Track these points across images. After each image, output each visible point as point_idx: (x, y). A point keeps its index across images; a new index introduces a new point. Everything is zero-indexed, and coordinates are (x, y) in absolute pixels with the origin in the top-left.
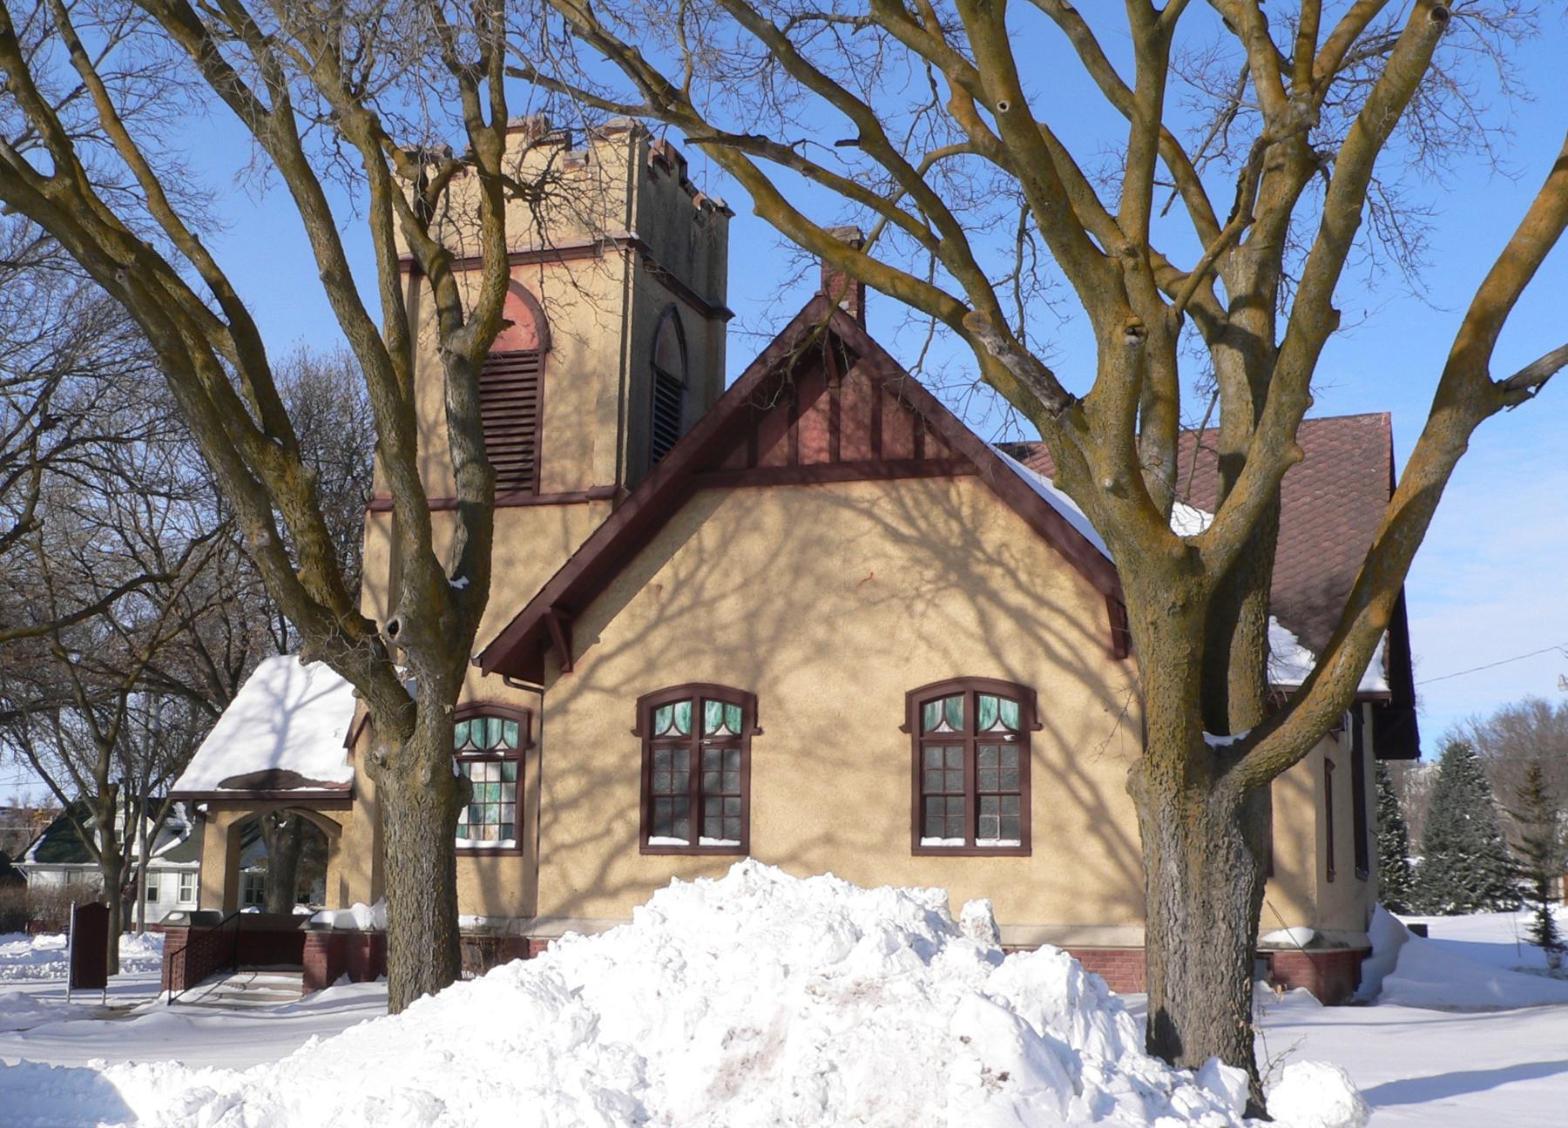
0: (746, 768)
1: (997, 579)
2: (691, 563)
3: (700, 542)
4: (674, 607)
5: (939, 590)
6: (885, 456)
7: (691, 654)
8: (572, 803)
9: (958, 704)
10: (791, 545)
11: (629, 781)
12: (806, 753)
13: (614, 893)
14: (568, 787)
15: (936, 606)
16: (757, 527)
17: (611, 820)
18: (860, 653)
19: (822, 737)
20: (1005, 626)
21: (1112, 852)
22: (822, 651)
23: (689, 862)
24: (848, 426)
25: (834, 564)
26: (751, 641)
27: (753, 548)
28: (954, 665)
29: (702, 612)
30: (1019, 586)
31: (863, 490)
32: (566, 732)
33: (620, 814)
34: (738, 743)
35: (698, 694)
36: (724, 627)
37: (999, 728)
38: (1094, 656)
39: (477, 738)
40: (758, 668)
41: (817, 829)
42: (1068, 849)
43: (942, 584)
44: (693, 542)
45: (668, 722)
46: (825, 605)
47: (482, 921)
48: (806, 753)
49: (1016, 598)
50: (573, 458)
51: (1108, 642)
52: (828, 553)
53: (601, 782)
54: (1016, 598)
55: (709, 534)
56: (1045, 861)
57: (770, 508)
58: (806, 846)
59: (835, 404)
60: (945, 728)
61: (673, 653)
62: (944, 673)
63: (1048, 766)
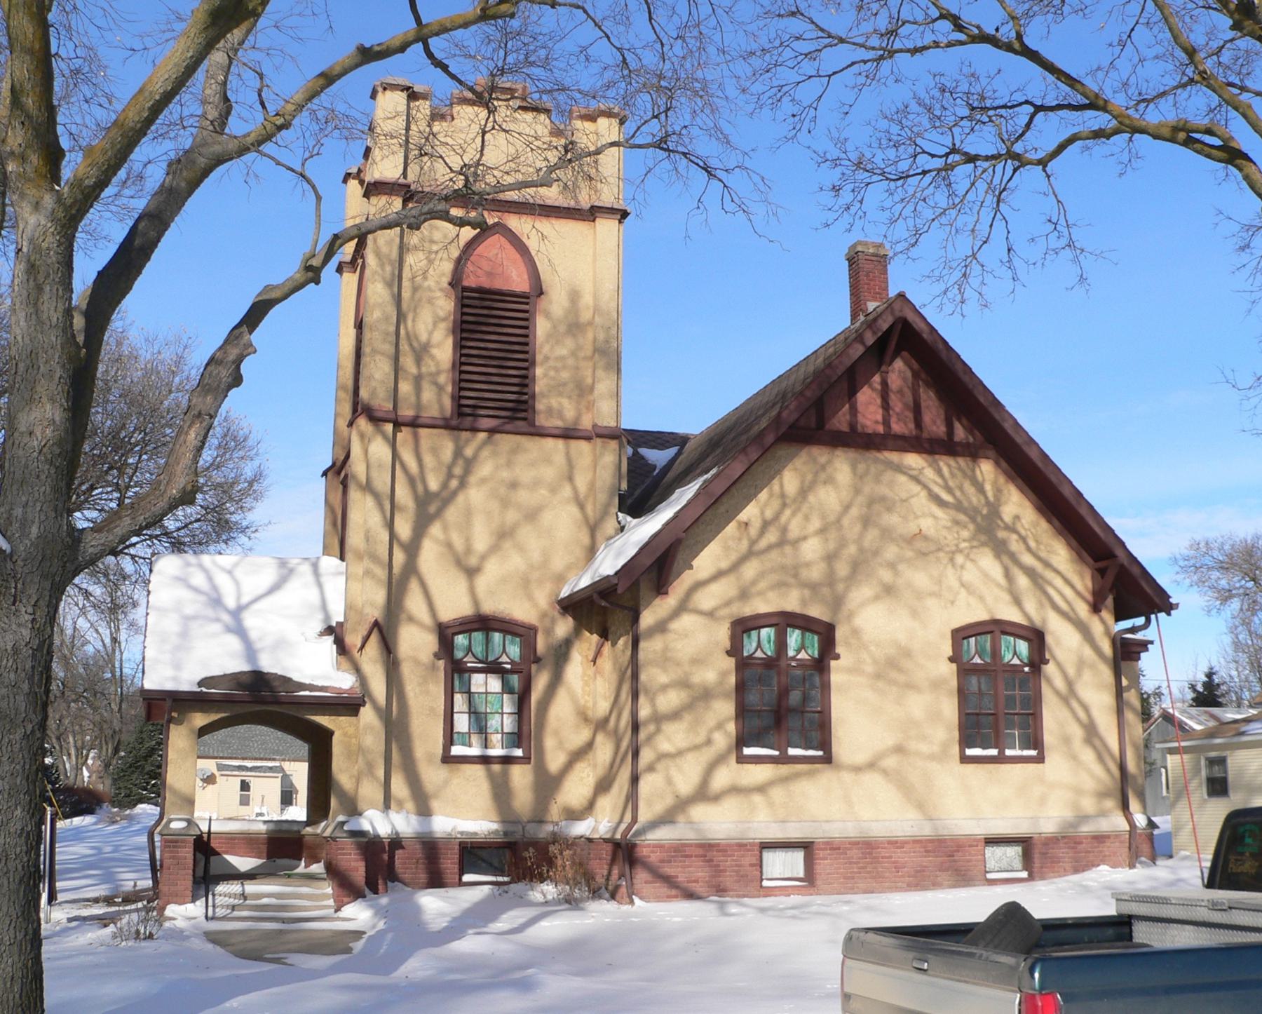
0: (826, 687)
1: (1015, 545)
2: (776, 504)
3: (782, 486)
4: (763, 543)
5: (972, 547)
6: (925, 435)
7: (781, 585)
8: (675, 715)
9: (986, 641)
10: (861, 499)
11: (726, 696)
12: (878, 676)
13: (716, 798)
14: (670, 700)
15: (972, 560)
16: (830, 481)
17: (711, 731)
18: (919, 595)
19: (892, 663)
20: (1023, 581)
21: (1100, 759)
22: (888, 590)
23: (784, 769)
24: (897, 404)
25: (892, 519)
26: (831, 580)
27: (828, 498)
28: (989, 611)
29: (788, 549)
30: (1029, 549)
31: (913, 460)
32: (666, 649)
33: (720, 726)
34: (821, 665)
35: (785, 621)
36: (808, 565)
37: (1016, 661)
38: (1083, 610)
39: (478, 649)
40: (837, 603)
41: (890, 741)
42: (1074, 758)
43: (975, 543)
44: (775, 484)
45: (754, 645)
46: (891, 552)
47: (494, 826)
48: (878, 676)
49: (1028, 559)
50: (570, 397)
51: (1089, 597)
52: (889, 510)
53: (705, 695)
54: (1028, 559)
55: (789, 480)
56: (1056, 765)
57: (842, 466)
58: (881, 756)
59: (884, 384)
60: (977, 660)
61: (762, 585)
62: (981, 615)
63: (1057, 692)
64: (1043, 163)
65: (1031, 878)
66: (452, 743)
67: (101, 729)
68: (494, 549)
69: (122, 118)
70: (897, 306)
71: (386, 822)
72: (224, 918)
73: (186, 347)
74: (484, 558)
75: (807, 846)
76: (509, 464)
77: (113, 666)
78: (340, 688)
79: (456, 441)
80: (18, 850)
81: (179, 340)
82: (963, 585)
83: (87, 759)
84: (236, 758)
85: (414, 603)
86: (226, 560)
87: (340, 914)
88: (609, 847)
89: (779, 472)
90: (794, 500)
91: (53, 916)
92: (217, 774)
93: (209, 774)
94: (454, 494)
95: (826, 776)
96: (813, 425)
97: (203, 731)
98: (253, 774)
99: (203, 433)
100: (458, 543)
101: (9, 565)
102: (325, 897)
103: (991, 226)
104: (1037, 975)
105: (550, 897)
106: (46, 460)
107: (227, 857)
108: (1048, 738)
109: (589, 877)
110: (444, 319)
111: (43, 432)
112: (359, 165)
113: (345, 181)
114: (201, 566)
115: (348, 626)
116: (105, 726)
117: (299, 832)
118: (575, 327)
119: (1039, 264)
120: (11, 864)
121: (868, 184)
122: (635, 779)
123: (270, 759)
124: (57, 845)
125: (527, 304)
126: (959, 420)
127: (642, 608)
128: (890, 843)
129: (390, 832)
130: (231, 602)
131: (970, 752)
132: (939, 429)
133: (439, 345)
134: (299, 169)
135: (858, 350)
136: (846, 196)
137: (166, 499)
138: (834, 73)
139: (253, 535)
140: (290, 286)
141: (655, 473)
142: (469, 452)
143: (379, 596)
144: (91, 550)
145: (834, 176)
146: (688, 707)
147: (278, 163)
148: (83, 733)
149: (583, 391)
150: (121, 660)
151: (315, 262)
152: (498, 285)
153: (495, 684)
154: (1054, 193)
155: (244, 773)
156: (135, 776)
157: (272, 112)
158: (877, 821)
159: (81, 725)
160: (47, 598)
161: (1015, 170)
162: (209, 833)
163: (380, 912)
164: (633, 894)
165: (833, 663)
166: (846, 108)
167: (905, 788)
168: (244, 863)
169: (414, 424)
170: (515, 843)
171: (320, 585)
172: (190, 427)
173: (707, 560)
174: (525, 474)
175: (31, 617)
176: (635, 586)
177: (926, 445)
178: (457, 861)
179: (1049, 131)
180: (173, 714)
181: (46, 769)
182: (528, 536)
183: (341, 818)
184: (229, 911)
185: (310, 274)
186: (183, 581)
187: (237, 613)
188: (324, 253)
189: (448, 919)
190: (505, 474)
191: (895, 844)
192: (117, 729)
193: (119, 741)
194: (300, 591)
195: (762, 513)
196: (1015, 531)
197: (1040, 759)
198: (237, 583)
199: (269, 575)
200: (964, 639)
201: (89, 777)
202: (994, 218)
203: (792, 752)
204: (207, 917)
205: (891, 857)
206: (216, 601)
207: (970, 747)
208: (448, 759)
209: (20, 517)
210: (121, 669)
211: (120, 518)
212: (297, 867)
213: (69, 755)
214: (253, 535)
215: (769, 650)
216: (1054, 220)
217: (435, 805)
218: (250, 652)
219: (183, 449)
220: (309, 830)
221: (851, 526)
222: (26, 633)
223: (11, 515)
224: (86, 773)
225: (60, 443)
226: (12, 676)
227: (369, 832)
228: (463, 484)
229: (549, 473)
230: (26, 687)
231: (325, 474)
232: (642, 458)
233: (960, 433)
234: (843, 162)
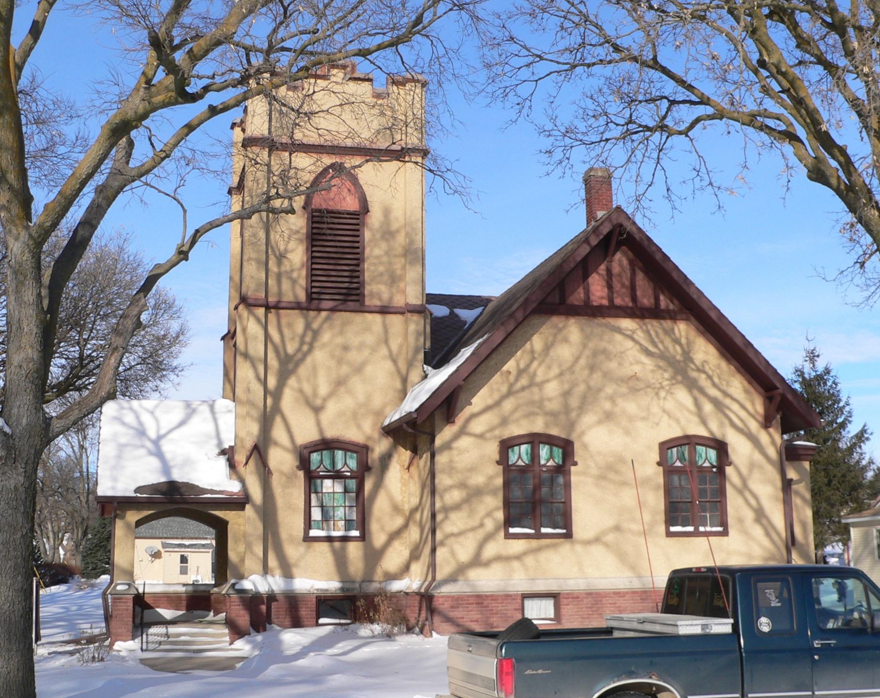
0: (568, 486)
1: (703, 380)
4: (518, 385)
7: (529, 415)
8: (457, 507)
10: (587, 352)
11: (493, 493)
12: (602, 477)
13: (487, 564)
14: (455, 496)
16: (566, 340)
17: (482, 519)
18: (631, 419)
19: (610, 468)
20: (708, 407)
21: (768, 534)
22: (608, 417)
23: (534, 543)
25: (613, 365)
26: (567, 410)
27: (564, 352)
28: (683, 429)
29: (535, 390)
30: (714, 385)
31: (627, 324)
32: (451, 461)
33: (489, 514)
34: (562, 470)
35: (535, 440)
36: (550, 400)
37: (707, 464)
38: (754, 426)
39: (327, 463)
40: (571, 425)
41: (610, 522)
43: (674, 382)
44: (528, 345)
45: (516, 456)
46: (609, 390)
48: (602, 477)
49: (713, 392)
50: (386, 284)
51: (761, 419)
54: (713, 392)
55: (537, 342)
58: (605, 533)
59: (609, 271)
60: (678, 464)
61: (517, 415)
64: (685, 133)
66: (310, 528)
67: (73, 517)
68: (331, 394)
69: (65, 188)
70: (614, 216)
71: (265, 583)
72: (154, 650)
73: (125, 240)
74: (325, 400)
75: (554, 596)
77: (81, 467)
78: (232, 492)
79: (306, 318)
80: (20, 599)
81: (120, 235)
82: (664, 411)
83: (62, 541)
84: (177, 538)
85: (279, 432)
86: (148, 404)
87: (233, 646)
88: (418, 598)
89: (529, 339)
90: (540, 355)
91: (40, 651)
92: (162, 550)
93: (156, 551)
94: (305, 355)
95: (565, 547)
96: (557, 301)
97: (139, 523)
98: (190, 550)
99: (119, 358)
100: (307, 388)
101: (11, 441)
102: (223, 635)
103: (654, 175)
104: (503, 651)
105: (376, 633)
106: (30, 381)
107: (158, 610)
108: (731, 521)
109: (404, 620)
110: (297, 232)
111: (28, 366)
112: (241, 118)
113: (232, 128)
114: (131, 409)
115: (237, 448)
116: (76, 515)
117: (209, 591)
118: (388, 234)
119: (690, 198)
120: (16, 607)
121: (572, 147)
122: (434, 550)
123: (203, 538)
124: (40, 606)
125: (358, 219)
126: (663, 293)
127: (436, 433)
128: (615, 593)
129: (267, 590)
130: (152, 434)
131: (673, 529)
132: (646, 299)
134: (172, 194)
135: (585, 250)
136: (558, 155)
137: (99, 398)
138: (540, 79)
139: (180, 374)
140: (169, 265)
141: (466, 327)
142: (315, 326)
143: (254, 428)
144: (56, 430)
145: (546, 143)
146: (467, 500)
147: (160, 191)
148: (59, 520)
149: (394, 279)
150: (87, 462)
151: (185, 249)
153: (339, 488)
154: (696, 151)
155: (183, 550)
156: (99, 554)
157: (158, 150)
158: (605, 578)
159: (57, 514)
160: (33, 459)
161: (668, 137)
162: (144, 593)
163: (255, 646)
164: (433, 630)
165: (573, 469)
166: (552, 99)
167: (622, 556)
168: (167, 614)
169: (277, 307)
170: (354, 597)
171: (215, 420)
172: (111, 355)
173: (479, 400)
174: (354, 340)
175: (24, 470)
176: (431, 416)
177: (638, 313)
178: (315, 609)
179: (685, 114)
180: (118, 512)
181: (34, 548)
182: (358, 385)
183: (233, 581)
184: (157, 645)
185: (182, 256)
186: (119, 420)
187: (156, 442)
188: (189, 242)
189: (300, 647)
190: (339, 340)
191: (618, 594)
192: (85, 517)
193: (87, 526)
194: (201, 423)
195: (518, 364)
196: (704, 372)
198: (157, 420)
199: (178, 415)
200: (668, 449)
201: (64, 555)
202: (655, 169)
203: (544, 530)
204: (142, 650)
205: (616, 603)
206: (141, 432)
207: (673, 526)
208: (307, 539)
209: (16, 413)
210: (88, 470)
211: (73, 410)
212: (207, 616)
213: (48, 538)
214: (180, 374)
215: (526, 459)
216: (698, 168)
217: (295, 571)
218: (166, 468)
219: (108, 368)
220: (216, 589)
221: (581, 373)
222: (21, 479)
223: (11, 412)
224: (62, 552)
225: (37, 371)
226: (14, 503)
227: (252, 590)
228: (310, 350)
229: (370, 339)
230: (22, 509)
231: (223, 338)
232: (457, 316)
233: (664, 302)
234: (554, 133)
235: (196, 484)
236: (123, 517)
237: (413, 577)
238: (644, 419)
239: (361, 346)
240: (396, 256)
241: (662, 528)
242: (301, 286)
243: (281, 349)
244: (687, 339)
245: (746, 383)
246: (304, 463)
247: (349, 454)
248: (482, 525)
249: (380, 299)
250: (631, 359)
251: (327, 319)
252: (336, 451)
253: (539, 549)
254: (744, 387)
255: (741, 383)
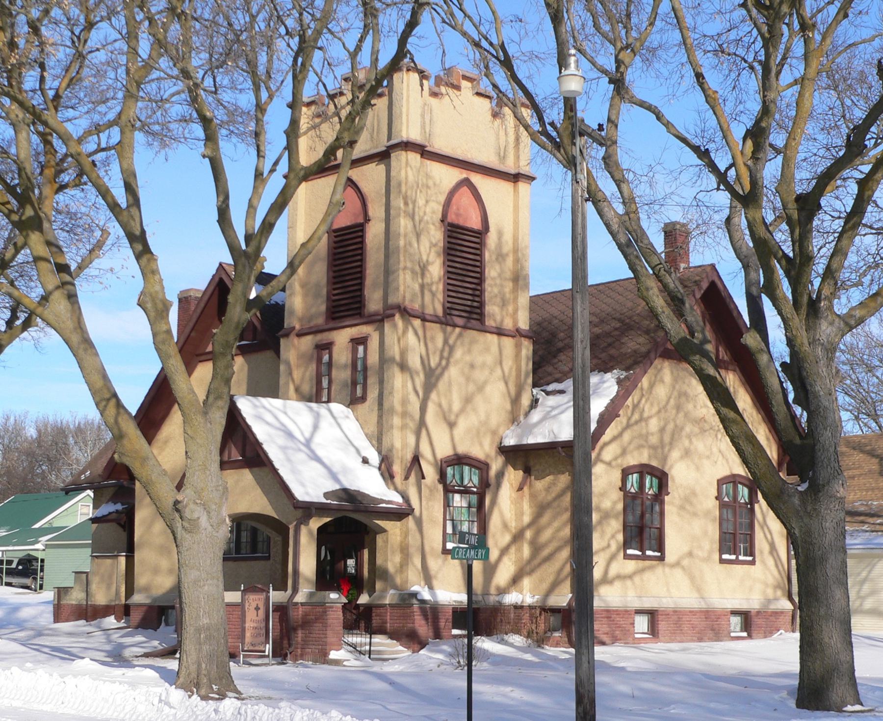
0: (662, 514)
7: (640, 447)
10: (676, 393)
11: (616, 517)
16: (662, 381)
22: (687, 453)
23: (641, 564)
29: (643, 424)
33: (613, 536)
40: (665, 459)
41: (686, 549)
50: (499, 306)
61: (632, 447)
65: (750, 636)
68: (462, 410)
74: (457, 416)
76: (469, 351)
79: (444, 332)
110: (435, 245)
128: (691, 612)
133: (433, 263)
142: (451, 342)
152: (461, 223)
174: (479, 360)
190: (468, 358)
191: (692, 612)
197: (753, 563)
203: (649, 553)
205: (691, 621)
217: (435, 583)
227: (430, 600)
229: (489, 359)
235: (367, 492)
236: (307, 524)
237: (525, 592)
238: (708, 457)
239: (484, 365)
240: (506, 279)
241: (716, 556)
242: (439, 300)
243: (426, 362)
244: (734, 388)
245: (767, 430)
246: (442, 477)
247: (473, 469)
248: (609, 546)
249: (495, 321)
250: (701, 402)
251: (460, 335)
252: (464, 467)
253: (642, 571)
254: (766, 434)
255: (765, 431)
